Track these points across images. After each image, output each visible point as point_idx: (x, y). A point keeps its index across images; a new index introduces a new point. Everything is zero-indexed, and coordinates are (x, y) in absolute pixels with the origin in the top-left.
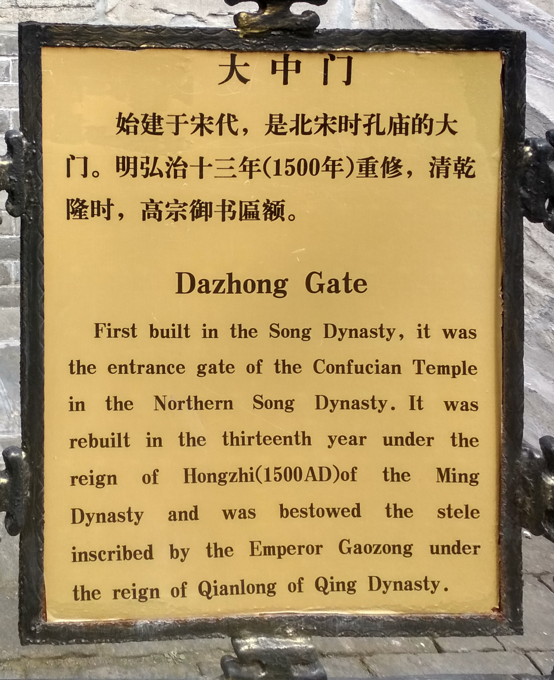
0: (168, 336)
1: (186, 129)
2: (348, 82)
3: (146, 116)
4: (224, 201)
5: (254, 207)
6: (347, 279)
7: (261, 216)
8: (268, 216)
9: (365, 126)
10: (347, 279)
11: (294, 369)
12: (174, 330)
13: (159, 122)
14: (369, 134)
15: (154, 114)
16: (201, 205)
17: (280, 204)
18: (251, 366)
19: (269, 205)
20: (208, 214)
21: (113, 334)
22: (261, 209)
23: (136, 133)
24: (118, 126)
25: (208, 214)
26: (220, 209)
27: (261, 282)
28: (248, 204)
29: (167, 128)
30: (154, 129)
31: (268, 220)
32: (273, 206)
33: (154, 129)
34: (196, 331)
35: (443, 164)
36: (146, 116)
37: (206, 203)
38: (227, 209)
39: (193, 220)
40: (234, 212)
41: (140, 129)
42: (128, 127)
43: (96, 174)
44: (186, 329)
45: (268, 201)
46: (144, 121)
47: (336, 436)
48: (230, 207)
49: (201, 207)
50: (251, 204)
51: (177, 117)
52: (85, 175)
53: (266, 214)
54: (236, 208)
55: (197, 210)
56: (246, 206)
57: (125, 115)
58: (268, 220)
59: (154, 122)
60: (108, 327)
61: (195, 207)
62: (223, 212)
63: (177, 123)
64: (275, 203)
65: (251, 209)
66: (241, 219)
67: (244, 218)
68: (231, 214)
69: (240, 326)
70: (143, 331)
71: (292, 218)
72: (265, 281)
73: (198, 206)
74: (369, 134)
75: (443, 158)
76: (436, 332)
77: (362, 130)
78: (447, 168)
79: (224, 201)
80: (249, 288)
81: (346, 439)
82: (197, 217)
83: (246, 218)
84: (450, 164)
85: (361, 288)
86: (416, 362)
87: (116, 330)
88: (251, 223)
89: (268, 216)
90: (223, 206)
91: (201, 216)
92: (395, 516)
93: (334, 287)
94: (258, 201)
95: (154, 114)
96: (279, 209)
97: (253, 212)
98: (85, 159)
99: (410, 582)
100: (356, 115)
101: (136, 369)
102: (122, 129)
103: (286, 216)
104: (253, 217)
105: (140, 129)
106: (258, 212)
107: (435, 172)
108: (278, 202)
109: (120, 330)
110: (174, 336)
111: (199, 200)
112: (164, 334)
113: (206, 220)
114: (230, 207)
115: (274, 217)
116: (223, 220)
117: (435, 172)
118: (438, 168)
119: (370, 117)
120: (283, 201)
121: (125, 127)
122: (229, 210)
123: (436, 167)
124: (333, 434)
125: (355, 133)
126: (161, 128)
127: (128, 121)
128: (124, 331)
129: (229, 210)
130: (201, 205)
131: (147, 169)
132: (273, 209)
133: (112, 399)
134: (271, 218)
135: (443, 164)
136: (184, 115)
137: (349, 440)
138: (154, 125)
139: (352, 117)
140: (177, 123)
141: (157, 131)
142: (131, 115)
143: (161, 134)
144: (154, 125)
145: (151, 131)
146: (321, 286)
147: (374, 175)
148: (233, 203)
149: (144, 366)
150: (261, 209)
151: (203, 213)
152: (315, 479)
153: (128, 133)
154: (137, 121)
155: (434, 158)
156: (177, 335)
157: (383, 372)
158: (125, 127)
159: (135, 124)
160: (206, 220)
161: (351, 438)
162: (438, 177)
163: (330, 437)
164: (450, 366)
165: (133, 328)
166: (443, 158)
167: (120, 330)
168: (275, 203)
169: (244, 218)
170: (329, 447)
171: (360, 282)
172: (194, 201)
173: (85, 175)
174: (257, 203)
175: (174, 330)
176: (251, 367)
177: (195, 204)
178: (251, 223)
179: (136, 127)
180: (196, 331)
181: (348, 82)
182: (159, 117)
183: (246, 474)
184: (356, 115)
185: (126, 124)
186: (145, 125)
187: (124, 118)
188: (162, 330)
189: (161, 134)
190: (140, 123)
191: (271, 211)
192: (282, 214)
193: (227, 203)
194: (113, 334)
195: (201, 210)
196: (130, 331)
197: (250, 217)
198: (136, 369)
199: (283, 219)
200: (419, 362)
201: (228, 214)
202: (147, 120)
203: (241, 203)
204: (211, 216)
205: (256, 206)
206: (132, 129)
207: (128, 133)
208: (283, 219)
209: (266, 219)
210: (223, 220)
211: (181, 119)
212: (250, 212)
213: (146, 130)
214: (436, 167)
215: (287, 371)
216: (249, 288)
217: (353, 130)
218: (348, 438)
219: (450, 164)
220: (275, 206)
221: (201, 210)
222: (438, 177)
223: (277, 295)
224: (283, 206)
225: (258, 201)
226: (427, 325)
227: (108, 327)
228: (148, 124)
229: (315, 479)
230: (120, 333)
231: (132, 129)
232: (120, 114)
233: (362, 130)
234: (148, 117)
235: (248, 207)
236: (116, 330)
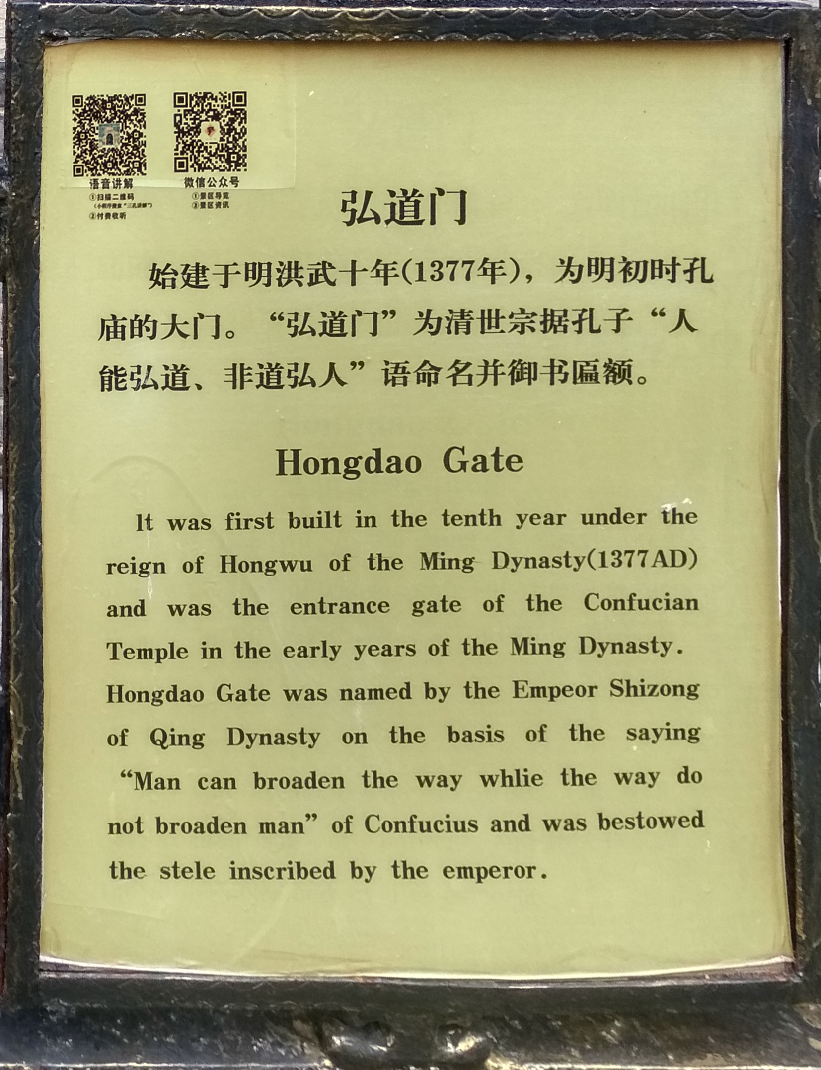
0: (312, 526)
1: (237, 281)
2: (462, 221)
3: (187, 266)
4: (552, 361)
5: (592, 368)
6: (496, 455)
7: (602, 378)
8: (611, 379)
9: (685, 272)
10: (496, 455)
11: (393, 564)
12: (320, 519)
13: (203, 273)
14: (691, 281)
15: (197, 264)
16: (522, 365)
17: (626, 364)
18: (188, 564)
19: (612, 365)
20: (533, 376)
21: (243, 525)
22: (601, 370)
23: (174, 286)
24: (152, 279)
25: (533, 376)
26: (549, 370)
27: (326, 461)
28: (584, 364)
29: (214, 279)
30: (197, 281)
31: (611, 383)
32: (617, 367)
33: (197, 281)
34: (348, 520)
35: (463, 318)
36: (187, 266)
37: (530, 364)
38: (556, 370)
39: (512, 383)
40: (566, 374)
41: (180, 281)
42: (164, 280)
43: (231, 335)
44: (337, 517)
45: (611, 360)
46: (184, 273)
47: (365, 646)
48: (561, 367)
49: (522, 369)
50: (588, 364)
51: (227, 267)
52: (217, 337)
53: (607, 377)
54: (569, 369)
55: (518, 373)
56: (581, 367)
57: (161, 267)
58: (611, 383)
59: (197, 274)
60: (236, 517)
61: (514, 368)
62: (552, 373)
63: (227, 274)
64: (620, 363)
65: (588, 369)
66: (575, 382)
67: (579, 381)
68: (562, 377)
69: (404, 512)
70: (281, 520)
71: (642, 380)
72: (332, 459)
73: (519, 367)
74: (691, 281)
75: (463, 311)
76: (160, 524)
77: (682, 277)
78: (468, 323)
79: (552, 361)
80: (311, 468)
81: (293, 650)
82: (518, 380)
83: (582, 380)
84: (472, 318)
85: (515, 466)
86: (111, 646)
87: (247, 521)
88: (588, 387)
89: (611, 379)
90: (552, 366)
91: (523, 379)
92: (582, 739)
93: (481, 465)
94: (597, 360)
95: (197, 264)
96: (624, 370)
97: (591, 374)
98: (217, 317)
99: (571, 821)
100: (674, 259)
101: (326, 608)
102: (157, 282)
103: (634, 378)
104: (591, 379)
105: (180, 281)
106: (597, 374)
107: (453, 329)
108: (623, 362)
109: (336, 604)
110: (320, 526)
111: (520, 360)
112: (308, 524)
113: (530, 383)
114: (561, 367)
115: (618, 380)
116: (552, 383)
117: (453, 329)
118: (457, 323)
119: (692, 261)
120: (630, 360)
121: (160, 280)
122: (560, 372)
123: (453, 323)
124: (361, 644)
125: (673, 281)
126: (205, 280)
127: (164, 273)
128: (257, 522)
129: (560, 372)
130: (522, 365)
131: (296, 327)
132: (617, 371)
133: (535, 598)
134: (614, 381)
135: (463, 318)
136: (235, 264)
137: (297, 651)
138: (197, 277)
139: (668, 261)
140: (227, 274)
141: (201, 284)
142: (168, 265)
143: (206, 287)
144: (197, 277)
145: (194, 284)
146: (464, 465)
147: (499, 330)
148: (565, 363)
149: (336, 604)
150: (601, 370)
151: (526, 376)
152: (665, 565)
153: (164, 288)
154: (176, 273)
155: (451, 311)
156: (324, 524)
157: (541, 566)
158: (160, 280)
159: (173, 276)
160: (530, 383)
161: (299, 649)
162: (457, 333)
163: (358, 647)
164: (461, 558)
165: (269, 518)
166: (463, 311)
167: (251, 520)
168: (620, 363)
169: (579, 381)
170: (356, 659)
171: (514, 459)
172: (514, 361)
173: (217, 337)
174: (596, 363)
175: (320, 519)
176: (188, 565)
177: (515, 365)
178: (589, 387)
179: (174, 280)
180: (348, 520)
181: (462, 221)
182: (203, 267)
183: (635, 687)
184: (674, 259)
185: (161, 277)
186: (185, 277)
187: (159, 270)
188: (305, 519)
189: (206, 287)
190: (180, 275)
191: (615, 373)
192: (629, 376)
193: (557, 363)
194: (243, 525)
195: (522, 372)
196: (265, 522)
197: (586, 380)
198: (326, 608)
199: (630, 382)
200: (115, 645)
201: (558, 377)
202: (188, 272)
203: (575, 363)
204: (535, 379)
205: (595, 367)
206: (168, 283)
207: (164, 288)
208: (630, 382)
209: (607, 382)
210: (552, 383)
211: (232, 270)
212: (586, 374)
213: (187, 283)
214: (453, 323)
215: (384, 566)
216: (311, 468)
217: (670, 276)
218: (296, 649)
219: (472, 318)
220: (620, 366)
221: (522, 372)
222: (457, 333)
223: (348, 476)
224: (629, 366)
225: (597, 360)
226: (337, 512)
227: (236, 517)
228: (189, 275)
229: (665, 565)
230: (252, 524)
231: (168, 283)
232: (155, 265)
233: (682, 277)
234: (190, 268)
235: (585, 368)
236: (247, 521)
